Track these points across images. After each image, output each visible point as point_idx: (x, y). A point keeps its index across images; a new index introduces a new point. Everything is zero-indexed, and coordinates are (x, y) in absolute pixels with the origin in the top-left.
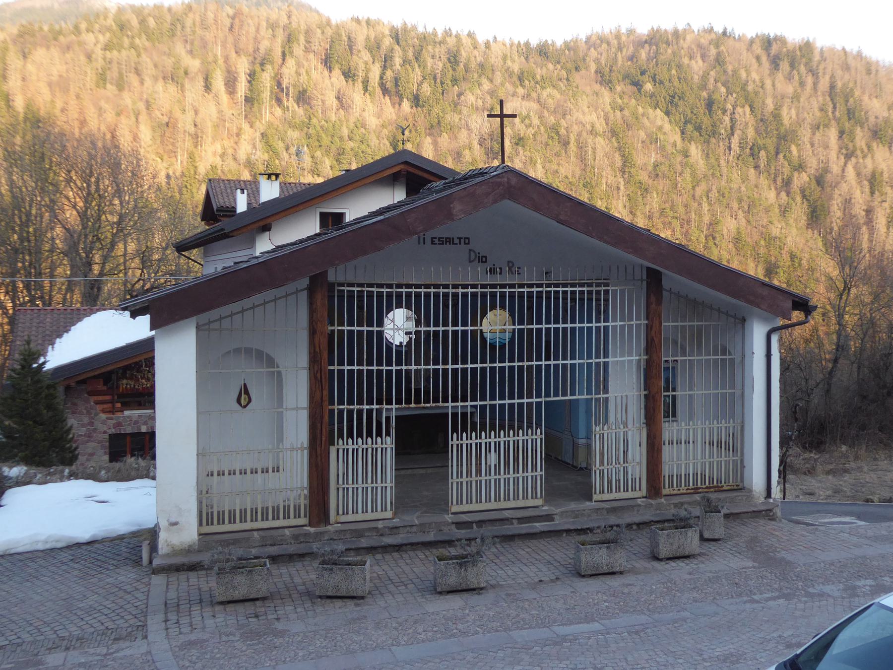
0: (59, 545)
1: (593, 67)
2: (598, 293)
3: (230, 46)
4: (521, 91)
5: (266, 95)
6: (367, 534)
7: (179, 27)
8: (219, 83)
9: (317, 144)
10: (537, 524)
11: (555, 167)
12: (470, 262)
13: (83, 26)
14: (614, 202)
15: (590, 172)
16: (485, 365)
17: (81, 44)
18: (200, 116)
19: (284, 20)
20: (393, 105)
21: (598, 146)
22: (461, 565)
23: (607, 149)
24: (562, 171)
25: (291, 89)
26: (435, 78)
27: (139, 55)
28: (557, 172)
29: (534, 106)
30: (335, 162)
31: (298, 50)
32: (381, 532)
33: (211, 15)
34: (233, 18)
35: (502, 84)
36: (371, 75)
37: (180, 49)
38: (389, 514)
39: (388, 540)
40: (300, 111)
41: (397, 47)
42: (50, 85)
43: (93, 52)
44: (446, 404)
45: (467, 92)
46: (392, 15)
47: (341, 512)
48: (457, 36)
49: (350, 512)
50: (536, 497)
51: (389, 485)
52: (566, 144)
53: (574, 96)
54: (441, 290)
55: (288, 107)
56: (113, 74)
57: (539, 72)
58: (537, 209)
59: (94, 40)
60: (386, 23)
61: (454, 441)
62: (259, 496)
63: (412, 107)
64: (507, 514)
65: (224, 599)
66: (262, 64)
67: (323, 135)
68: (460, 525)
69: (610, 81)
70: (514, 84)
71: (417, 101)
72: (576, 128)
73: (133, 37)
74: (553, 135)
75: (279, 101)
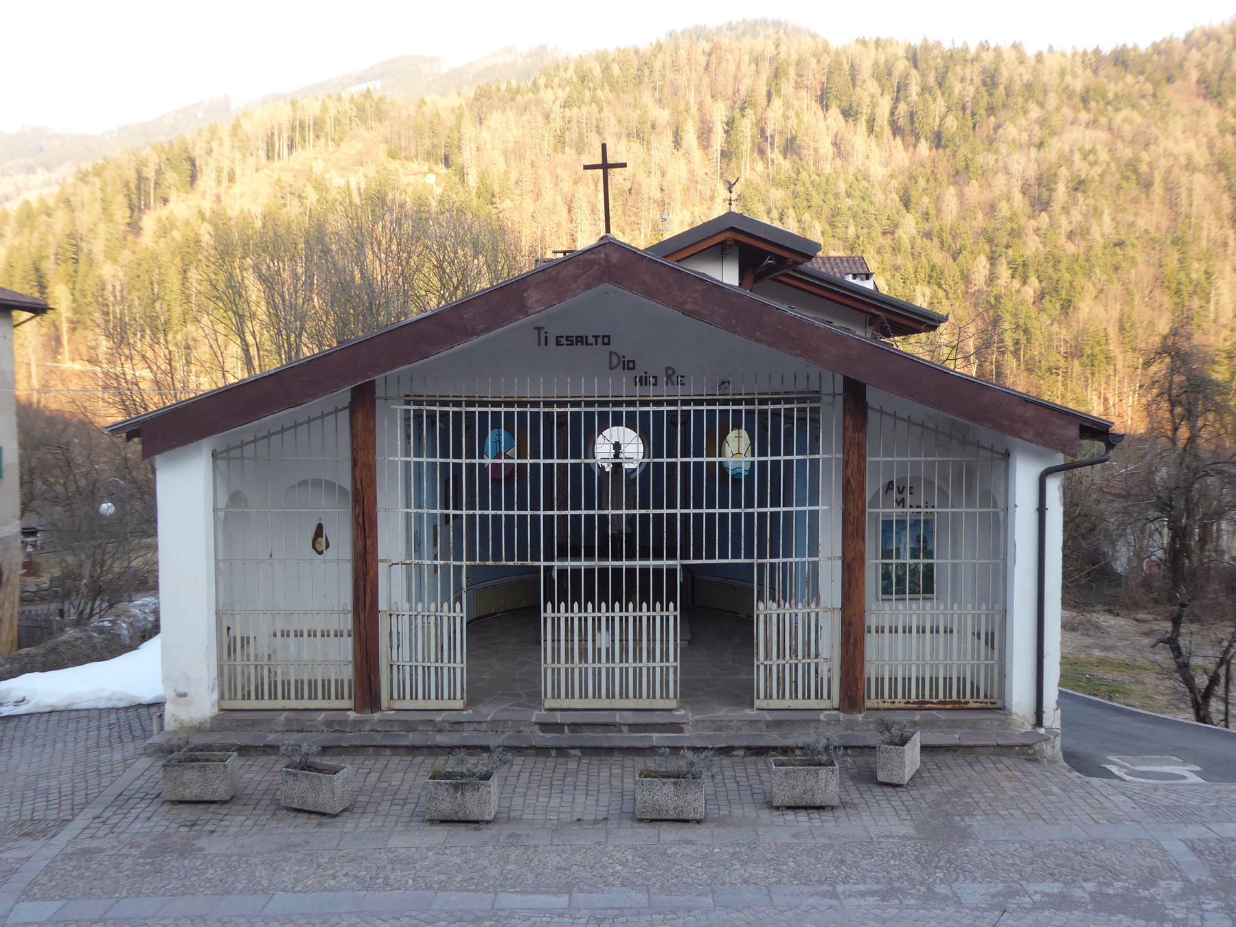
0: (121, 704)
1: (1194, 75)
2: (763, 413)
3: (705, 90)
4: (1084, 116)
5: (746, 147)
6: (420, 728)
7: (647, 72)
8: (690, 137)
9: (805, 204)
10: (655, 735)
11: (1129, 217)
12: (611, 368)
13: (542, 82)
14: (1219, 265)
15: (1183, 223)
16: (591, 512)
17: (539, 103)
18: (668, 178)
19: (771, 51)
20: (906, 147)
21: (1197, 186)
22: (456, 787)
23: (1211, 188)
24: (1141, 223)
25: (777, 138)
26: (964, 108)
27: (600, 111)
28: (1132, 224)
29: (1103, 135)
30: (827, 226)
31: (787, 87)
32: (439, 727)
33: (683, 53)
34: (710, 55)
35: (1058, 109)
36: (878, 111)
37: (648, 99)
38: (459, 704)
39: (442, 739)
40: (786, 164)
41: (913, 72)
42: (505, 153)
43: (551, 111)
44: (536, 563)
45: (1008, 123)
46: (908, 32)
47: (395, 696)
48: (997, 50)
49: (408, 697)
50: (668, 697)
51: (458, 665)
52: (1147, 185)
53: (1163, 118)
54: (529, 409)
55: (773, 161)
56: (572, 135)
57: (1112, 89)
58: (649, 294)
59: (552, 97)
60: (901, 41)
61: (548, 614)
62: (292, 669)
63: (931, 149)
64: (618, 718)
65: (173, 798)
66: (743, 109)
67: (814, 193)
68: (545, 726)
69: (1219, 94)
70: (1075, 109)
71: (938, 140)
72: (1163, 163)
73: (595, 89)
74: (1129, 174)
75: (762, 152)
